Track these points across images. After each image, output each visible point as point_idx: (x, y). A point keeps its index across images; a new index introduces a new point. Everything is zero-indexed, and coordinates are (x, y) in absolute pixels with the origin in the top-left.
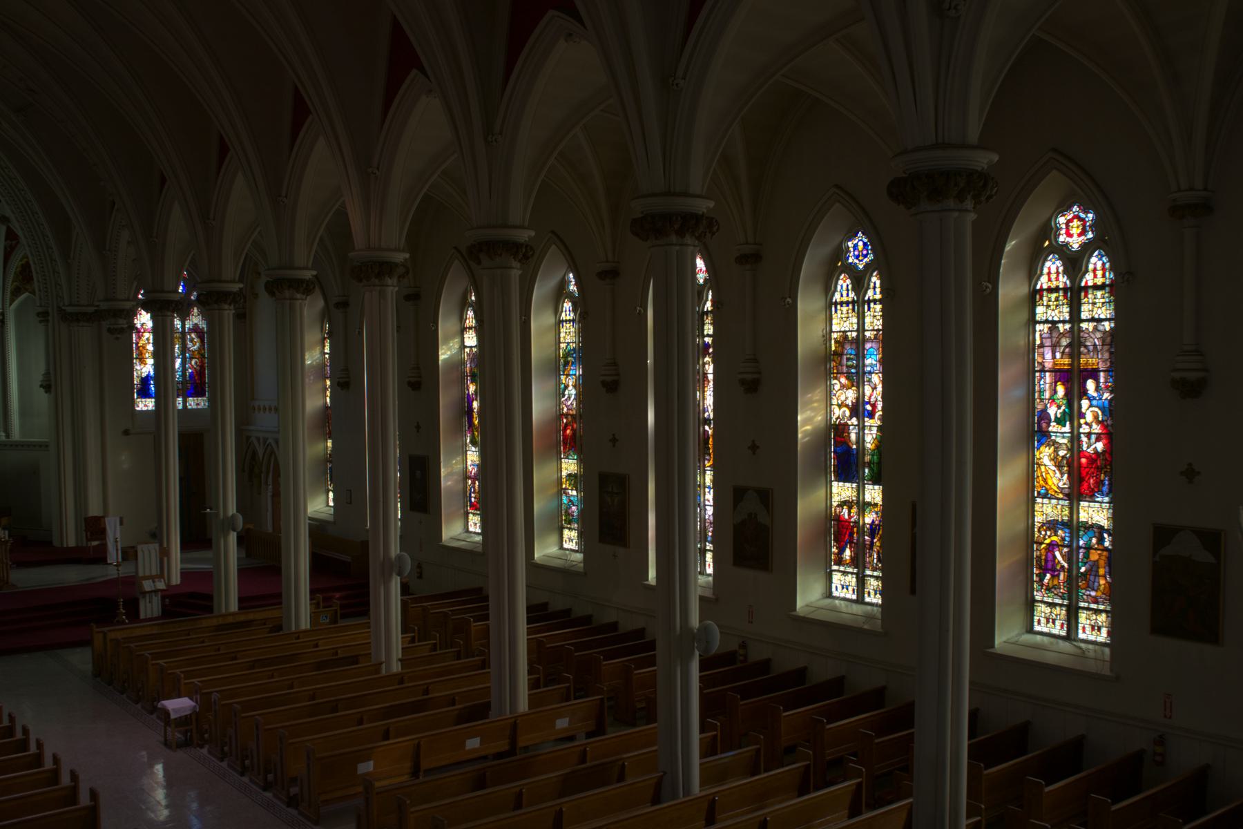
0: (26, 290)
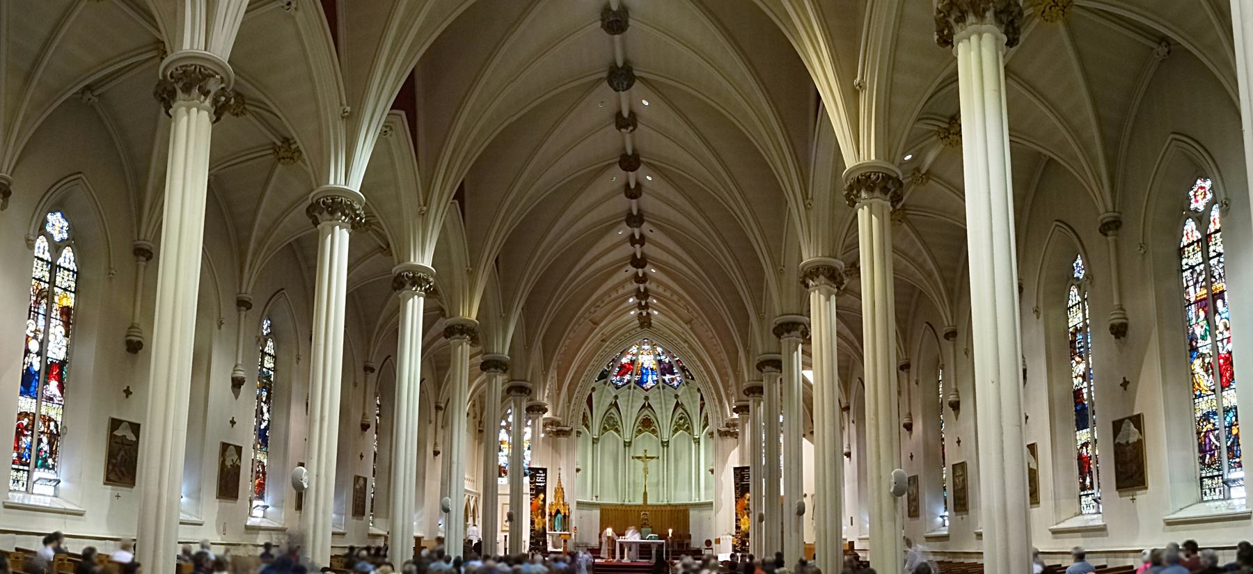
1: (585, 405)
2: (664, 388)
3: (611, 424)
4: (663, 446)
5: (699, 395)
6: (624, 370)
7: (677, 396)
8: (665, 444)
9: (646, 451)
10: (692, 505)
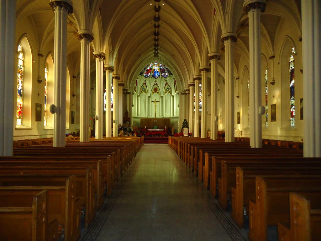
1: (135, 84)
2: (162, 78)
3: (143, 90)
4: (161, 98)
6: (148, 71)
7: (166, 81)
8: (162, 97)
10: (171, 118)
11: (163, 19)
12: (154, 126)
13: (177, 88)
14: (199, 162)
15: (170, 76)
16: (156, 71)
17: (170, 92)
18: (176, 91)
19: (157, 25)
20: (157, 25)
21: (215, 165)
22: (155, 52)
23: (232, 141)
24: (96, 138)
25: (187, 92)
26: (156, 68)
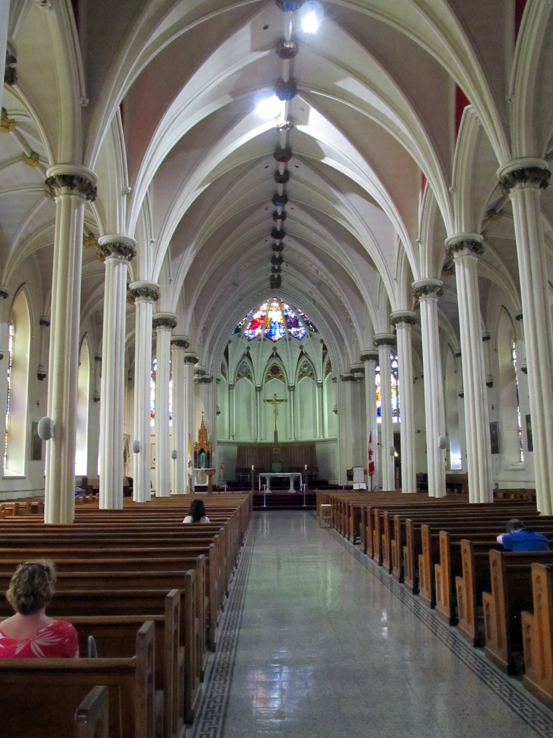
0: (306, 375)
4: (290, 391)
5: (322, 345)
8: (292, 389)
9: (275, 395)
11: (294, 200)
12: (273, 464)
13: (329, 365)
14: (420, 556)
15: (311, 335)
16: (275, 323)
17: (312, 375)
18: (327, 372)
19: (280, 213)
20: (280, 213)
21: (469, 563)
22: (273, 276)
23: (485, 500)
24: (134, 500)
25: (356, 375)
26: (276, 316)
